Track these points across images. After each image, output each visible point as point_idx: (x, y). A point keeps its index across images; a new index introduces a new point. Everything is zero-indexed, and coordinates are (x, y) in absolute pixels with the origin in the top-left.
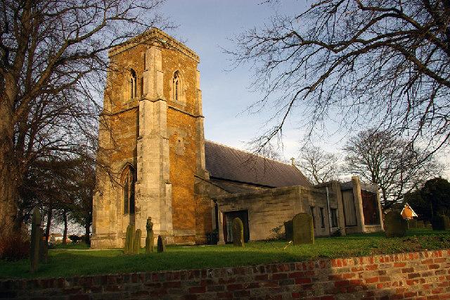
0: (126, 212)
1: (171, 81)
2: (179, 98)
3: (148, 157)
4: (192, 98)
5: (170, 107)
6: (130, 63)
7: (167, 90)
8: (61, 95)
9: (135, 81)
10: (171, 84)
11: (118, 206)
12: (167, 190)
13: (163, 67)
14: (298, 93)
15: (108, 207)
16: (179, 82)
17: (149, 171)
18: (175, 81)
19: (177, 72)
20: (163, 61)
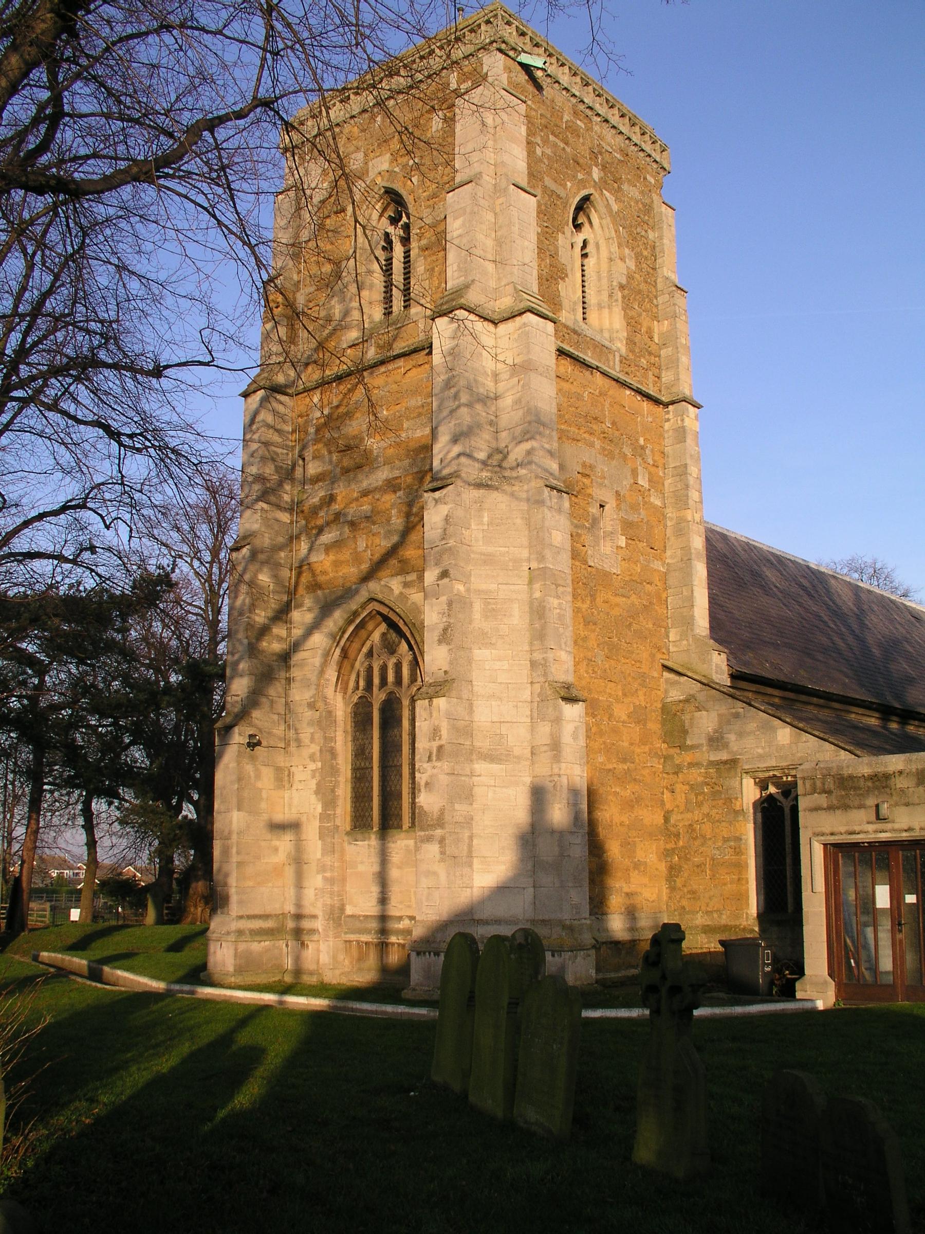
0: (360, 822)
1: (562, 241)
2: (592, 316)
3: (465, 469)
4: (645, 322)
5: (561, 352)
6: (382, 163)
7: (552, 274)
8: (17, 199)
9: (406, 241)
10: (570, 258)
11: (329, 803)
12: (568, 730)
13: (532, 175)
14: (79, 422)
15: (278, 799)
16: (590, 249)
17: (485, 640)
18: (579, 239)
19: (583, 205)
20: (531, 153)
